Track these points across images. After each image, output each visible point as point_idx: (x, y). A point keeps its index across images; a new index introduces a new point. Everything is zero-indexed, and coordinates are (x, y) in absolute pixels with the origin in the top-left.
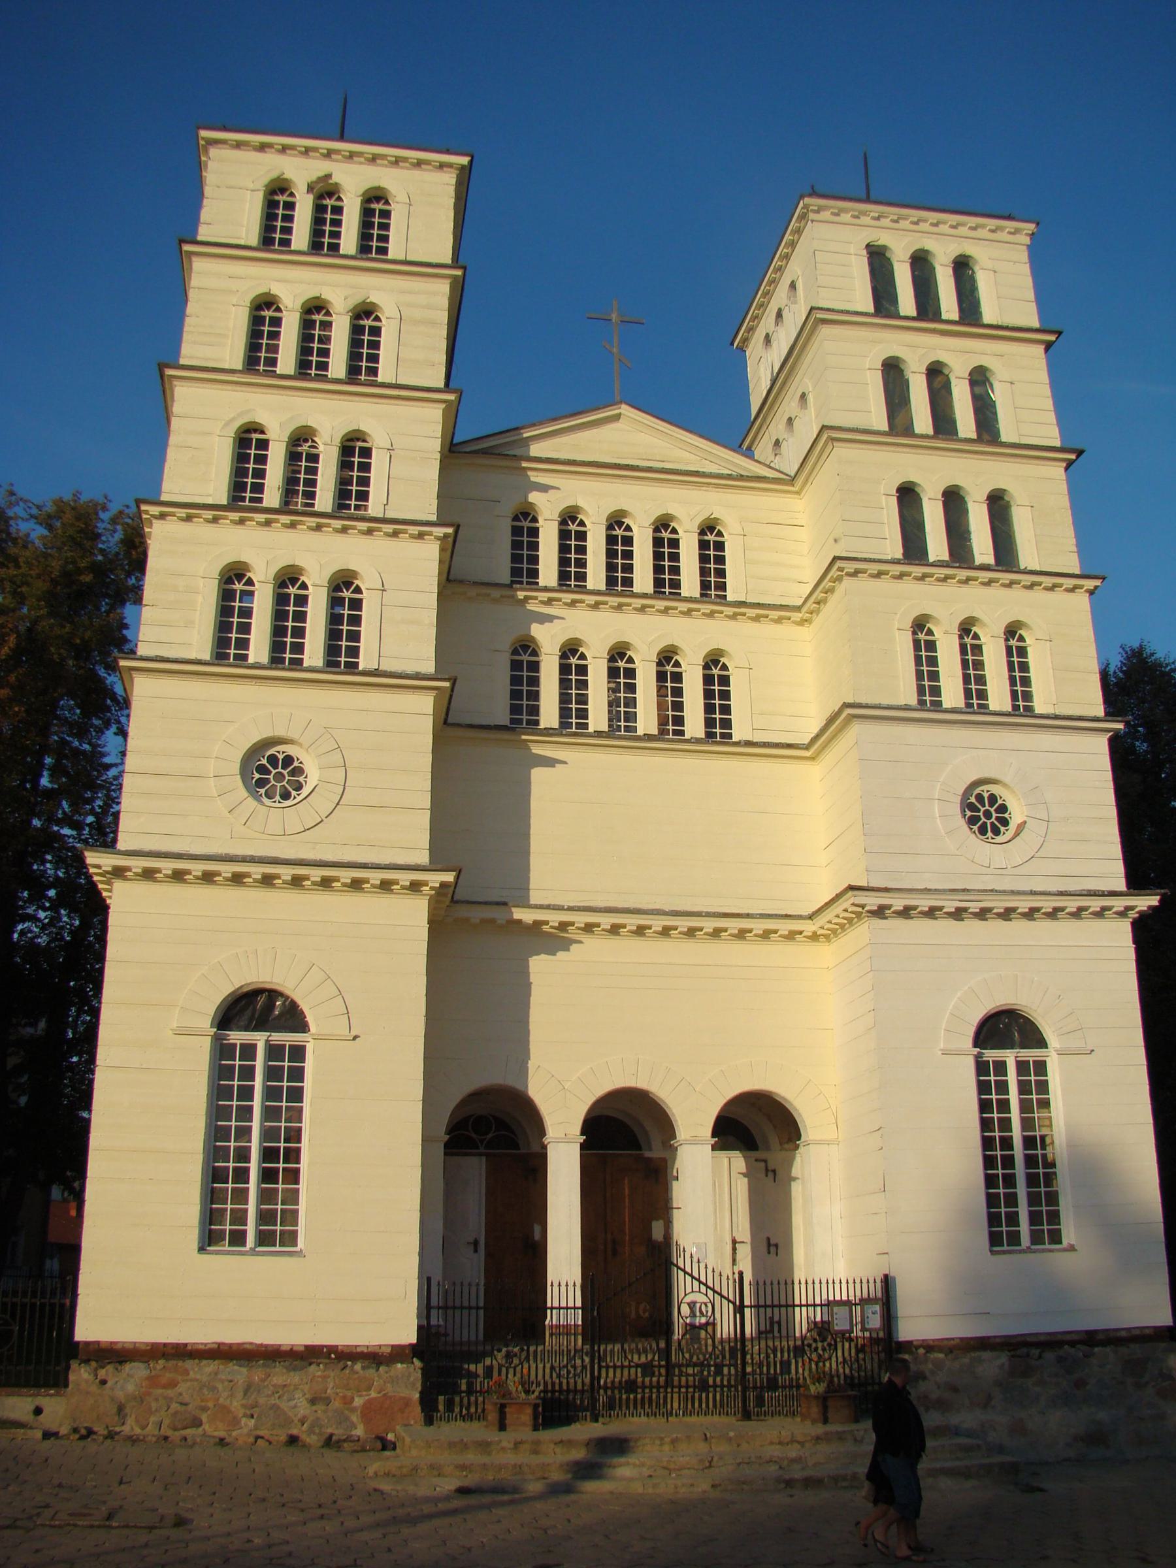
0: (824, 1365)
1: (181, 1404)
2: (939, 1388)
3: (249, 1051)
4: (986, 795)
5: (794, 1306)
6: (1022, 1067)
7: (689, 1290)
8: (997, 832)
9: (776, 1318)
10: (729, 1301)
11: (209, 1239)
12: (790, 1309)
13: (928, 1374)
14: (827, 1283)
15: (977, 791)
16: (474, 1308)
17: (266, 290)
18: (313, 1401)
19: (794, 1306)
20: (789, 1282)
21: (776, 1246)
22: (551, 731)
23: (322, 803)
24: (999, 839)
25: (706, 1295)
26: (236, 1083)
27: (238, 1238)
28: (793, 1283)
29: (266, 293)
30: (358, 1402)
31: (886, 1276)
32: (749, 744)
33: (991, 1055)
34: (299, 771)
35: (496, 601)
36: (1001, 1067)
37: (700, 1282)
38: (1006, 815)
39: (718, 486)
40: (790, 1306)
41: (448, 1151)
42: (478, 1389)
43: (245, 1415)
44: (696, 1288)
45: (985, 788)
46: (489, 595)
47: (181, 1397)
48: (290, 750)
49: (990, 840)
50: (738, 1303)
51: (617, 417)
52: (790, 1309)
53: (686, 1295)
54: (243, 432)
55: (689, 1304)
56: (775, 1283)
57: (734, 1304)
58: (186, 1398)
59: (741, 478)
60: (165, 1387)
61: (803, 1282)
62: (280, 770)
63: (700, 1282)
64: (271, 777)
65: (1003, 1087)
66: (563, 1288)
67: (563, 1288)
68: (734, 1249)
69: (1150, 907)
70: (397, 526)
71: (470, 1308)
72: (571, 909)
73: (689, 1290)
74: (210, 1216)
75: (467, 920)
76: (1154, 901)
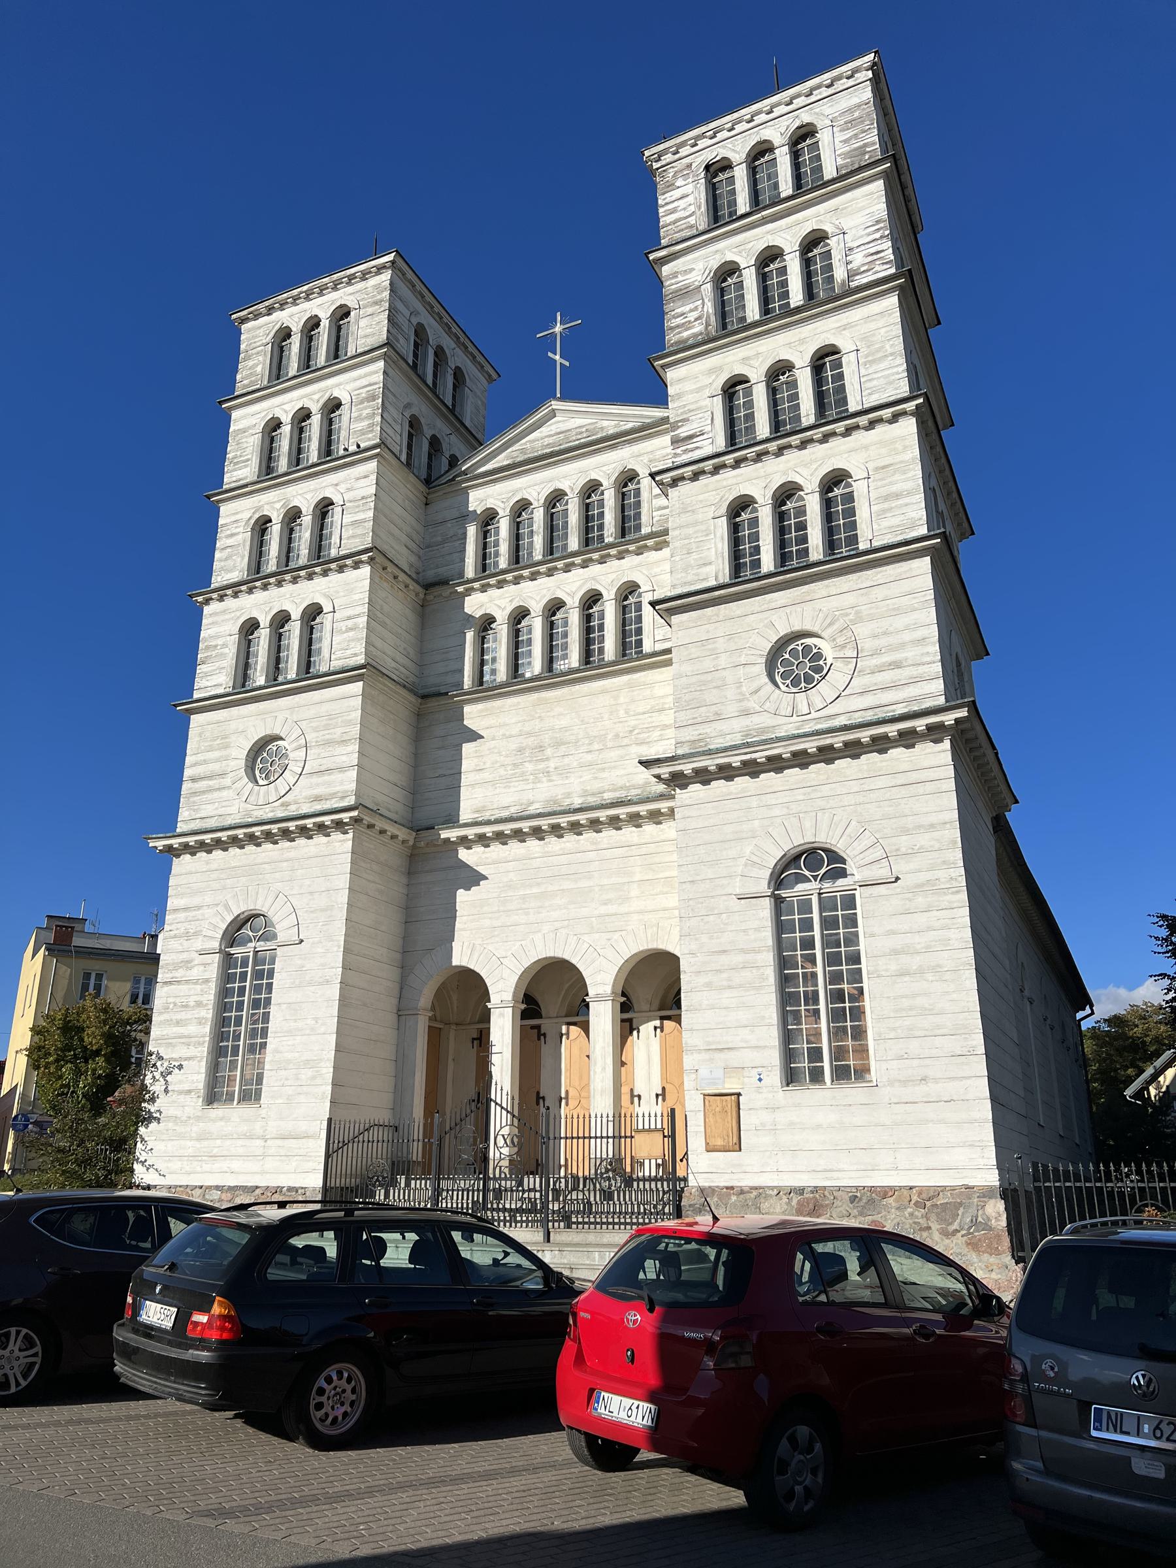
0: (668, 1186)
3: (805, 906)
5: (614, 1137)
11: (791, 1077)
19: (614, 1137)
21: (639, 1097)
23: (837, 678)
26: (798, 934)
27: (817, 1076)
34: (819, 656)
39: (630, 442)
42: (491, 1176)
47: (925, 1234)
51: (553, 415)
54: (818, 360)
62: (806, 661)
64: (809, 665)
66: (581, 1120)
67: (581, 1120)
74: (789, 1056)
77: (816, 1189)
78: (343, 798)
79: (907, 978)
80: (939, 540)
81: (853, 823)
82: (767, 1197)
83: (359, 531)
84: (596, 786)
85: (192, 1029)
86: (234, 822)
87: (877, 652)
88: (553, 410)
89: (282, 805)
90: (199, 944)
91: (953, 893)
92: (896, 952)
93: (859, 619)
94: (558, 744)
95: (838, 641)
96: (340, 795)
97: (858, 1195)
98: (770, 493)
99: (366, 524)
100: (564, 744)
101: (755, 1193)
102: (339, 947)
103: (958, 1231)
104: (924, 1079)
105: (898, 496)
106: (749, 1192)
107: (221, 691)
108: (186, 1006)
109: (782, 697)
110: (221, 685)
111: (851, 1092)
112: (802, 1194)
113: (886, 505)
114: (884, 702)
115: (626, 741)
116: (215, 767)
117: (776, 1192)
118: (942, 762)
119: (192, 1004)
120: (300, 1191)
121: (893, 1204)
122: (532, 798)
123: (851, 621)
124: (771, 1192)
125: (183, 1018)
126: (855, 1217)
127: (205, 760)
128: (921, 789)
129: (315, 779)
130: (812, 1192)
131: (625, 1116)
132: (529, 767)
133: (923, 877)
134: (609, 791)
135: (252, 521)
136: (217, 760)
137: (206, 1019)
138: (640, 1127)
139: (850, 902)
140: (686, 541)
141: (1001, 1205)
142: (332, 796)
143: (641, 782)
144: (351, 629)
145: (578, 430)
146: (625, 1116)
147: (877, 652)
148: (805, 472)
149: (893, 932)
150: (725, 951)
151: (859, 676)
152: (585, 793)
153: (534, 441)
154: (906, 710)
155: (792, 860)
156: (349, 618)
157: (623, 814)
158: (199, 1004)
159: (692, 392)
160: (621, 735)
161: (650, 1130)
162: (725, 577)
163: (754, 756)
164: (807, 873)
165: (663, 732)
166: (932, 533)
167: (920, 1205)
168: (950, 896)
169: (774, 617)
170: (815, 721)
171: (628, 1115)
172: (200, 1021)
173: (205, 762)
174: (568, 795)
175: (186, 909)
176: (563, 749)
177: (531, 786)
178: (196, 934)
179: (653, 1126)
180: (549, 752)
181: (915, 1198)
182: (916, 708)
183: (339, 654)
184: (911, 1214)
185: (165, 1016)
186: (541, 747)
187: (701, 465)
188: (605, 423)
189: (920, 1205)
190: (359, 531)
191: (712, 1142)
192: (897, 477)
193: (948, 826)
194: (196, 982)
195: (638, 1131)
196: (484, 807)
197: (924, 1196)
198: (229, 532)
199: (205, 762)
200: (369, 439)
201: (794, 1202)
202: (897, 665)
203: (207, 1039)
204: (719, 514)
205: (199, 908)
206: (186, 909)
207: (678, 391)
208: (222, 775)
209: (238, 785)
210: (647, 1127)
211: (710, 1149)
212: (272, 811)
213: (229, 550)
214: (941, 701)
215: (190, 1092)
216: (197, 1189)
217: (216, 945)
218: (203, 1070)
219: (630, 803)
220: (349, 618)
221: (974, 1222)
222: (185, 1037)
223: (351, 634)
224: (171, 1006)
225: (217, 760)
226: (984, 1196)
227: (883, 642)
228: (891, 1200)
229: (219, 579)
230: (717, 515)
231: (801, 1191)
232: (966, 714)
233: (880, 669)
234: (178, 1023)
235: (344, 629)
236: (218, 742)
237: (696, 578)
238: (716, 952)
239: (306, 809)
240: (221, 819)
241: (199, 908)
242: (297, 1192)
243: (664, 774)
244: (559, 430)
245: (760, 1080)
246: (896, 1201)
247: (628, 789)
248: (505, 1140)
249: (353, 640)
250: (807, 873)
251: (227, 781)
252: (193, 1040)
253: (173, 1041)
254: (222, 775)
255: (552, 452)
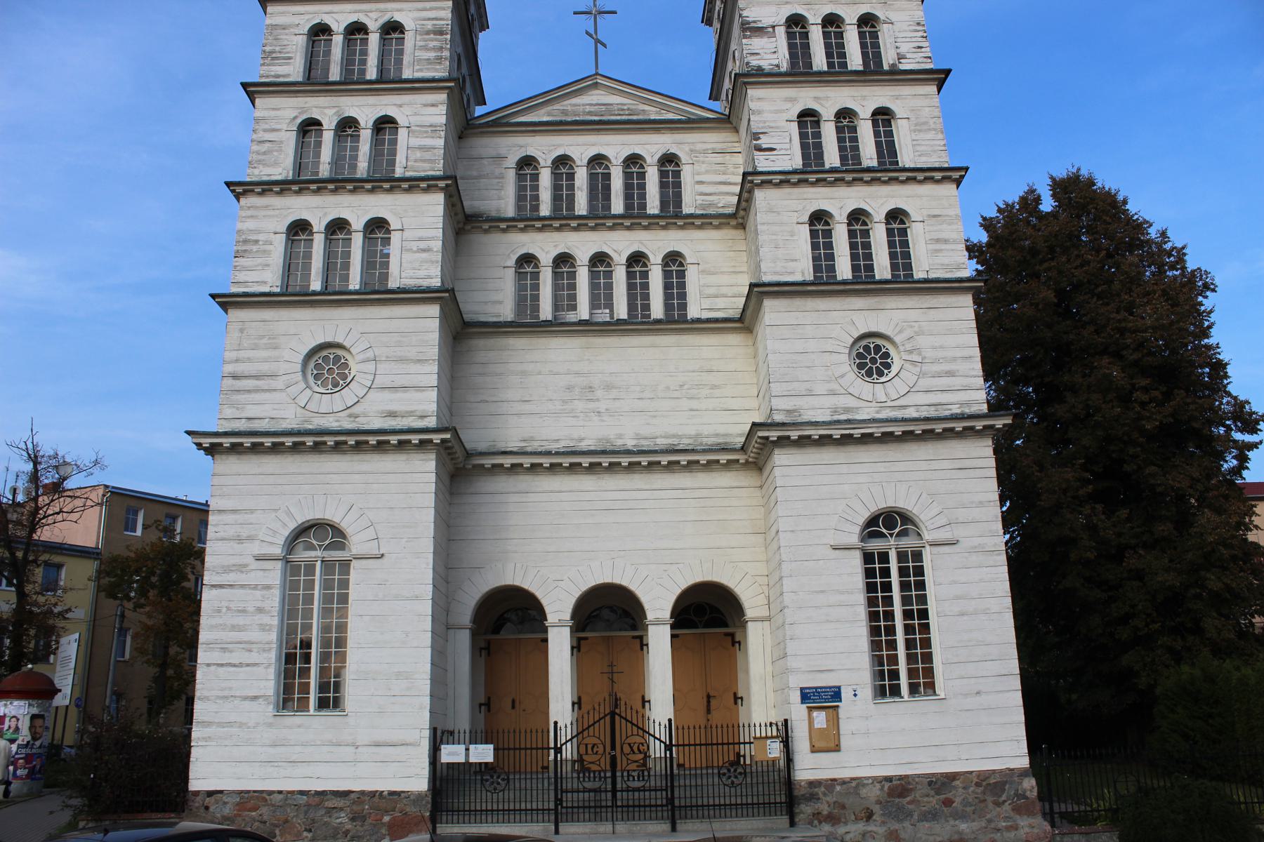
1: (261, 822)
2: (829, 806)
4: (872, 346)
6: (902, 556)
7: (629, 734)
8: (881, 374)
9: (742, 753)
10: (661, 741)
12: (545, 751)
13: (821, 796)
14: (760, 726)
15: (879, 342)
16: (523, 749)
17: (318, 21)
18: (353, 819)
20: (545, 731)
21: (742, 698)
22: (547, 323)
24: (883, 379)
25: (599, 738)
27: (303, 705)
28: (739, 727)
29: (320, 23)
30: (386, 819)
31: (786, 721)
32: (699, 321)
33: (875, 545)
35: (504, 231)
36: (884, 557)
37: (638, 727)
38: (889, 361)
40: (545, 748)
41: (677, 632)
43: (306, 830)
44: (635, 732)
45: (871, 340)
46: (604, 224)
48: (892, 352)
49: (875, 381)
50: (668, 743)
52: (545, 751)
53: (627, 737)
55: (629, 744)
56: (725, 726)
57: (665, 743)
58: (265, 818)
59: (689, 121)
60: (250, 810)
61: (757, 725)
63: (638, 727)
65: (886, 572)
66: (725, 729)
67: (725, 729)
68: (709, 702)
69: (1004, 425)
70: (413, 184)
71: (515, 749)
72: (557, 453)
73: (629, 734)
75: (483, 465)
76: (1009, 421)
77: (901, 778)
78: (422, 417)
79: (965, 618)
80: (983, 284)
81: (924, 495)
82: (864, 785)
83: (428, 155)
84: (646, 431)
85: (255, 635)
86: (291, 426)
87: (936, 361)
88: (597, 83)
89: (350, 416)
90: (257, 549)
91: (997, 555)
92: (958, 598)
93: (920, 333)
94: (608, 387)
95: (907, 346)
96: (418, 414)
97: (934, 779)
98: (845, 214)
99: (436, 151)
100: (616, 388)
101: (854, 784)
102: (428, 564)
103: (1005, 801)
104: (978, 693)
105: (946, 241)
106: (849, 782)
107: (266, 289)
108: (219, 611)
109: (863, 387)
110: (265, 283)
111: (923, 704)
112: (891, 781)
113: (938, 246)
114: (944, 401)
115: (676, 394)
116: (265, 368)
117: (870, 781)
118: (987, 455)
119: (251, 609)
120: (402, 795)
121: (961, 785)
122: (583, 435)
123: (915, 332)
124: (865, 782)
125: (241, 623)
126: (933, 796)
127: (249, 359)
128: (972, 473)
129: (387, 395)
130: (899, 780)
131: (744, 726)
132: (580, 405)
133: (977, 541)
134: (662, 437)
135: (299, 121)
136: (265, 360)
137: (271, 626)
138: (758, 735)
139: (918, 556)
140: (774, 237)
141: (1033, 782)
142: (410, 414)
143: (693, 433)
144: (424, 250)
145: (620, 107)
146: (744, 726)
147: (936, 361)
148: (873, 205)
149: (955, 582)
150: (822, 592)
151: (923, 377)
152: (638, 437)
153: (575, 105)
154: (959, 411)
155: (872, 521)
156: (421, 239)
157: (684, 460)
158: (260, 610)
159: (771, 112)
160: (672, 388)
161: (772, 737)
162: (809, 276)
163: (852, 432)
164: (884, 531)
165: (712, 391)
166: (663, 214)
167: (978, 785)
168: (995, 557)
169: (856, 317)
170: (890, 409)
171: (746, 725)
172: (264, 628)
173: (249, 360)
174: (620, 436)
175: (234, 511)
176: (614, 393)
177: (581, 423)
178: (251, 538)
179: (764, 735)
180: (599, 393)
181: (975, 780)
182: (967, 411)
183: (411, 273)
184: (973, 792)
185: (217, 621)
186: (591, 387)
187: (789, 177)
188: (647, 108)
189: (978, 785)
190: (428, 155)
191: (818, 745)
192: (945, 226)
193: (992, 504)
194: (255, 587)
195: (755, 738)
196: (532, 437)
197: (981, 778)
198: (267, 127)
199: (249, 360)
200: (436, 70)
201: (886, 788)
202: (950, 374)
203: (275, 646)
204: (802, 221)
205: (252, 511)
206: (234, 511)
207: (758, 108)
208: (273, 376)
209: (293, 390)
210: (769, 734)
211: (814, 750)
212: (337, 421)
213: (267, 145)
214: (984, 408)
215: (255, 698)
216: (276, 795)
217: (854, 539)
218: (272, 676)
219: (693, 451)
220: (421, 239)
221: (1016, 795)
222: (246, 642)
223: (424, 255)
224: (224, 610)
225: (265, 360)
226: (1021, 776)
227: (941, 354)
228: (957, 783)
229: (256, 172)
230: (800, 222)
231: (889, 779)
232: (1010, 422)
233: (939, 375)
234: (234, 628)
235: (415, 249)
236: (265, 341)
237: (784, 270)
238: (816, 592)
239: (377, 424)
240: (273, 422)
241: (252, 511)
242: (400, 796)
243: (773, 436)
244: (600, 102)
245: (855, 695)
246: (962, 783)
247: (680, 437)
248: (631, 748)
249: (426, 262)
250: (884, 531)
251: (279, 383)
252: (254, 646)
253: (230, 646)
254: (273, 376)
255: (600, 120)
